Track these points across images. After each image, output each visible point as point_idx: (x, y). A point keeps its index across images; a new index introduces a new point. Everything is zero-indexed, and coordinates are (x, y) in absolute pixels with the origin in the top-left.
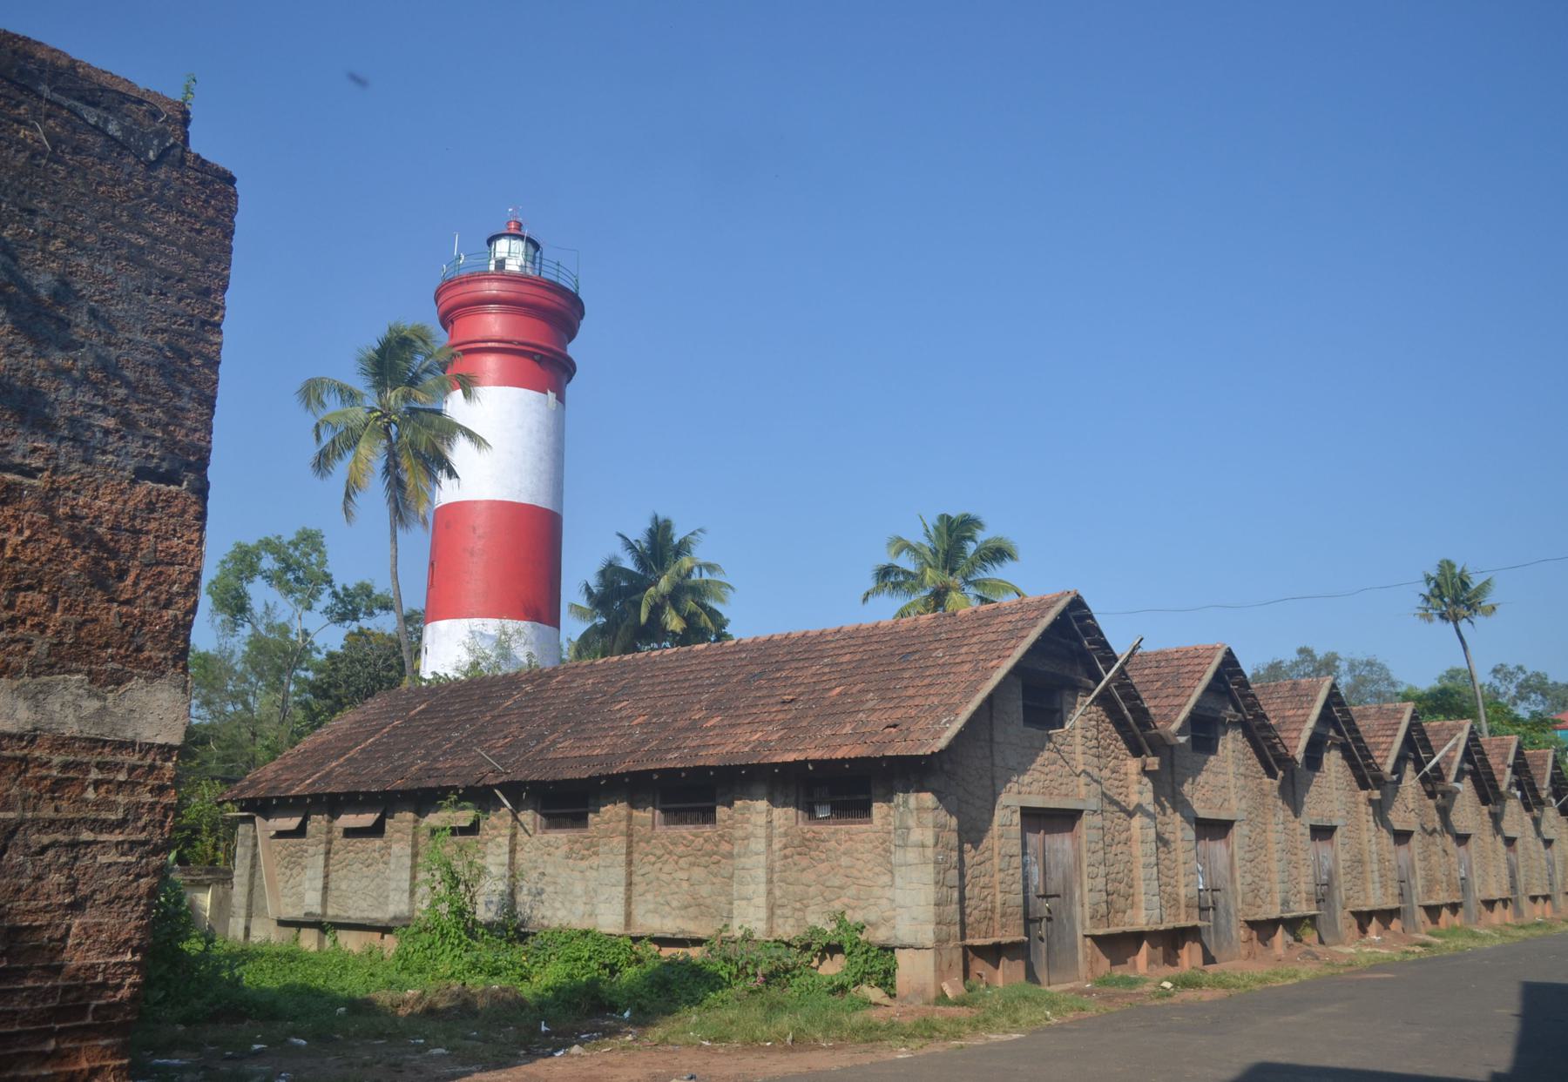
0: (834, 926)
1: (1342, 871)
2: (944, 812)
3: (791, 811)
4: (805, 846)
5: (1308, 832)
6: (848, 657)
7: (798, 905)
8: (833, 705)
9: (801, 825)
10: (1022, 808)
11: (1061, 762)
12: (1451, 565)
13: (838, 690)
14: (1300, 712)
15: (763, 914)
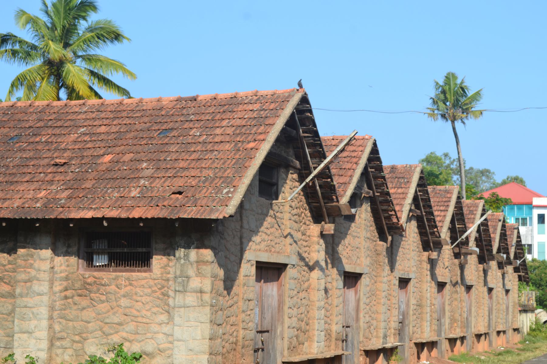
0: (112, 355)
1: (411, 313)
2: (216, 265)
3: (73, 260)
4: (86, 289)
5: (397, 283)
6: (103, 129)
7: (77, 338)
8: (109, 170)
9: (81, 271)
10: (257, 262)
11: (276, 226)
12: (454, 76)
13: (107, 158)
14: (400, 191)
15: (45, 345)
